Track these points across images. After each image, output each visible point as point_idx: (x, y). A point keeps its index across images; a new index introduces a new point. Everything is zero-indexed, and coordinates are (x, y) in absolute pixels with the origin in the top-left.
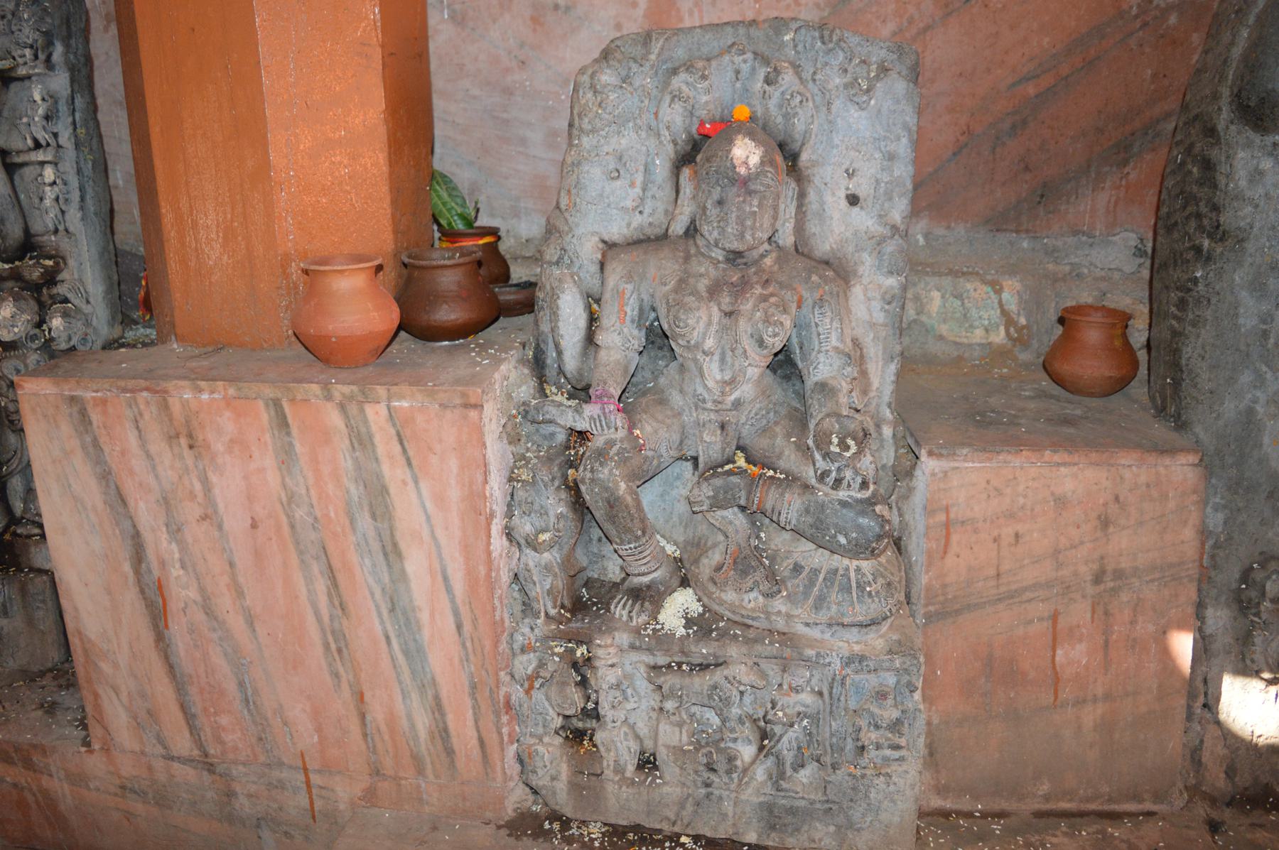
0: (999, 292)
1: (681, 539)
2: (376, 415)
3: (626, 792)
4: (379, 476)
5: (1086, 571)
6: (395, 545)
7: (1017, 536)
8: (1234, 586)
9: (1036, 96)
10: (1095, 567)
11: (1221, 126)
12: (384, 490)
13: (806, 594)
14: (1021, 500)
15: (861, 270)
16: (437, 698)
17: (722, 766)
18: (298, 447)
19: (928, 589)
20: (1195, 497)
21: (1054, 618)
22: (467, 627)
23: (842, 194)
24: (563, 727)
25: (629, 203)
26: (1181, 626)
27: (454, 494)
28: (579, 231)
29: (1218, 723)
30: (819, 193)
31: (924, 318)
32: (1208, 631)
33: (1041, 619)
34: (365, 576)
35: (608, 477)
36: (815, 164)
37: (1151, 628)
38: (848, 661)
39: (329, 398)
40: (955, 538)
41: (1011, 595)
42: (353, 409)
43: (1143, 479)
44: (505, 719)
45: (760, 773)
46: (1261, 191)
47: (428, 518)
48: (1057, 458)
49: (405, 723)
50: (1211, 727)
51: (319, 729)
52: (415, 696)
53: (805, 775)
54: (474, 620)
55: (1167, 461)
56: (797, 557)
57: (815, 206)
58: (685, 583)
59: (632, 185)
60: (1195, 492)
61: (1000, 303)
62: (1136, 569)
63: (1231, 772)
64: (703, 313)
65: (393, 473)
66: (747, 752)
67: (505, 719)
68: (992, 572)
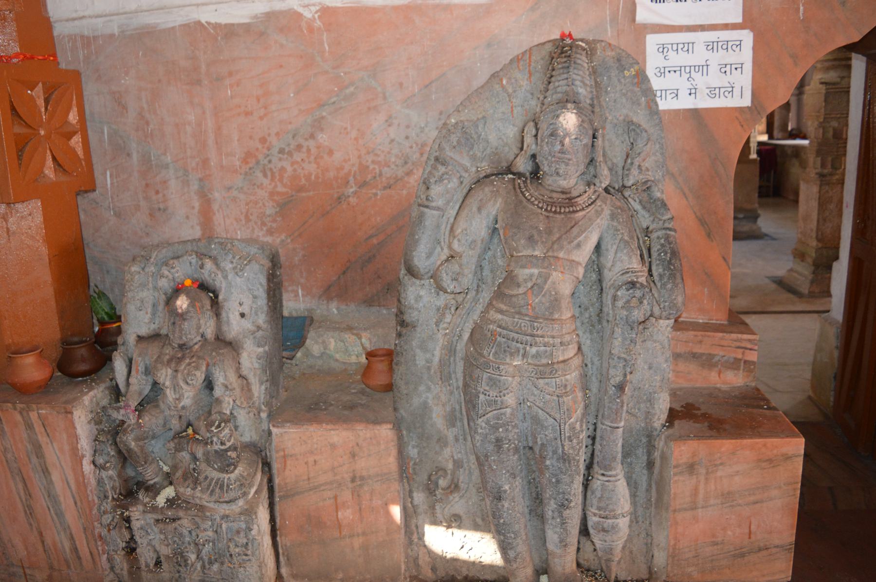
0: (360, 338)
1: (170, 464)
2: (33, 415)
3: (149, 576)
4: (38, 441)
5: (347, 477)
6: (47, 469)
7: (315, 461)
8: (425, 482)
9: (378, 244)
10: (351, 475)
11: (401, 276)
12: (40, 447)
13: (208, 489)
14: (315, 446)
15: (245, 346)
16: (71, 534)
17: (183, 564)
18: (6, 429)
19: (279, 485)
20: (393, 443)
21: (336, 498)
22: (79, 504)
23: (237, 314)
24: (126, 547)
25: (146, 321)
26: (394, 502)
27: (66, 448)
28: (129, 332)
29: (425, 546)
30: (227, 313)
31: (328, 352)
32: (415, 503)
33: (329, 498)
34: (37, 481)
35: (130, 440)
36: (225, 300)
37: (380, 502)
38: (222, 518)
39: (15, 409)
40: (288, 462)
41: (315, 488)
42: (25, 414)
43: (368, 435)
44: (99, 543)
45: (199, 566)
46: (421, 305)
47: (58, 458)
48: (329, 427)
49: (60, 545)
50: (422, 548)
51: (26, 549)
52: (62, 533)
53: (216, 567)
54: (81, 500)
55: (378, 427)
56: (207, 473)
57: (225, 319)
58: (171, 483)
59: (147, 313)
60: (393, 441)
61: (362, 345)
62: (370, 476)
63: (434, 569)
64: (164, 371)
65: (43, 439)
66: (193, 557)
67: (99, 543)
68: (306, 477)
